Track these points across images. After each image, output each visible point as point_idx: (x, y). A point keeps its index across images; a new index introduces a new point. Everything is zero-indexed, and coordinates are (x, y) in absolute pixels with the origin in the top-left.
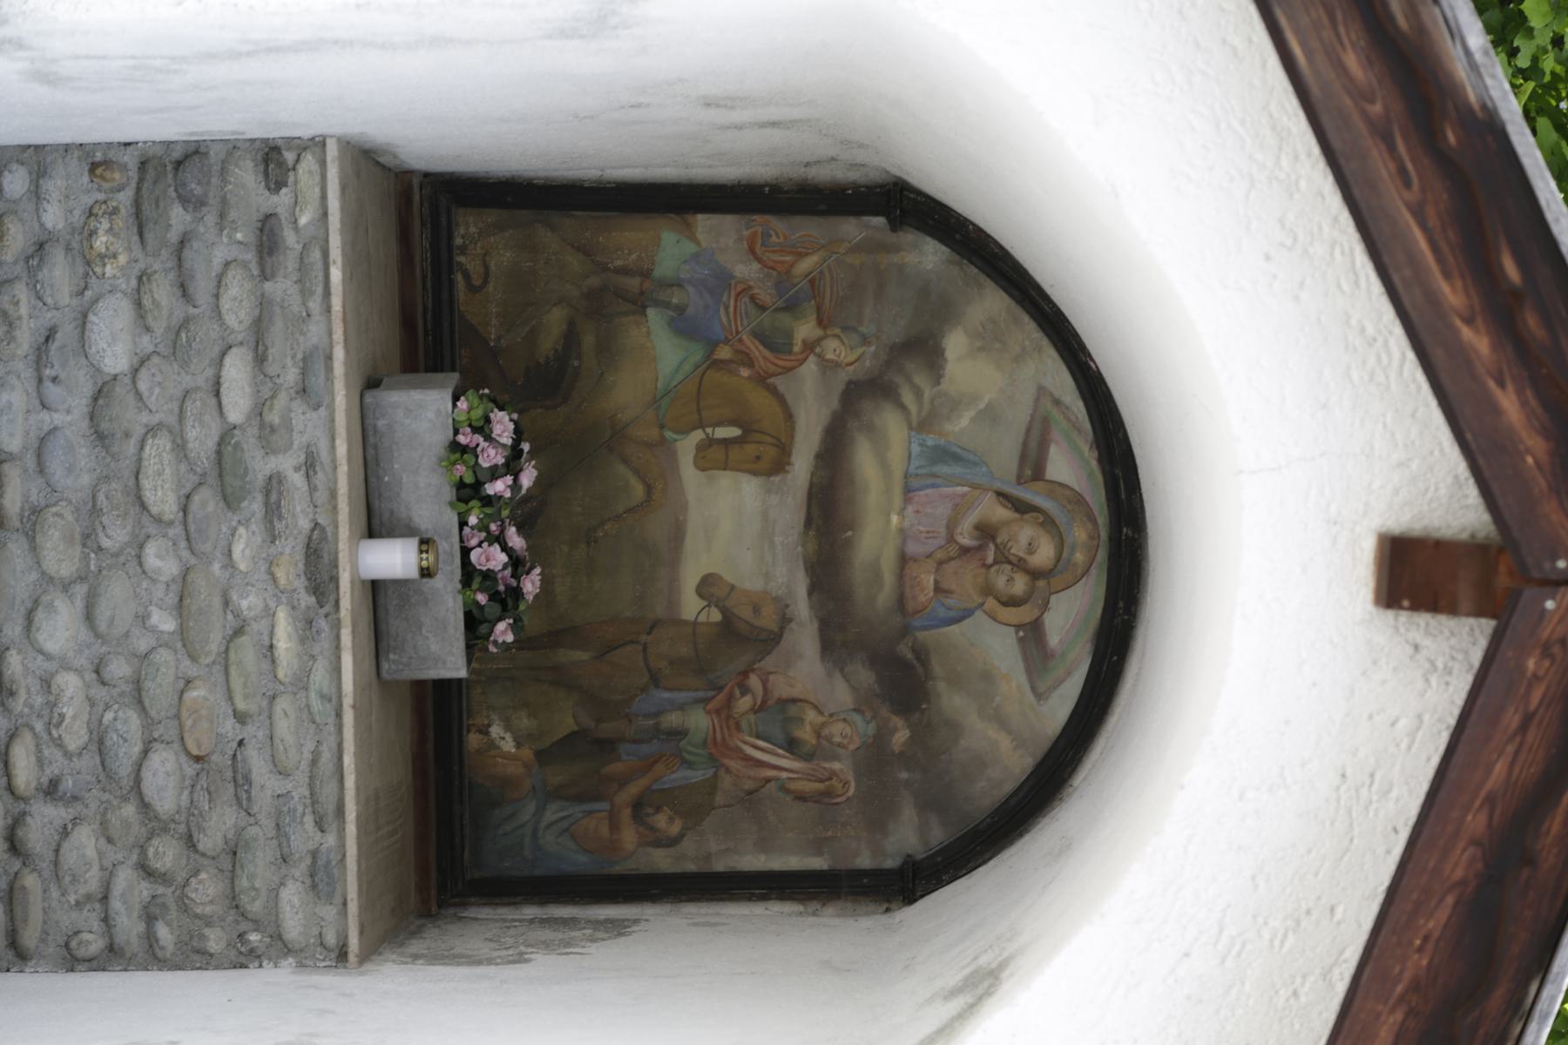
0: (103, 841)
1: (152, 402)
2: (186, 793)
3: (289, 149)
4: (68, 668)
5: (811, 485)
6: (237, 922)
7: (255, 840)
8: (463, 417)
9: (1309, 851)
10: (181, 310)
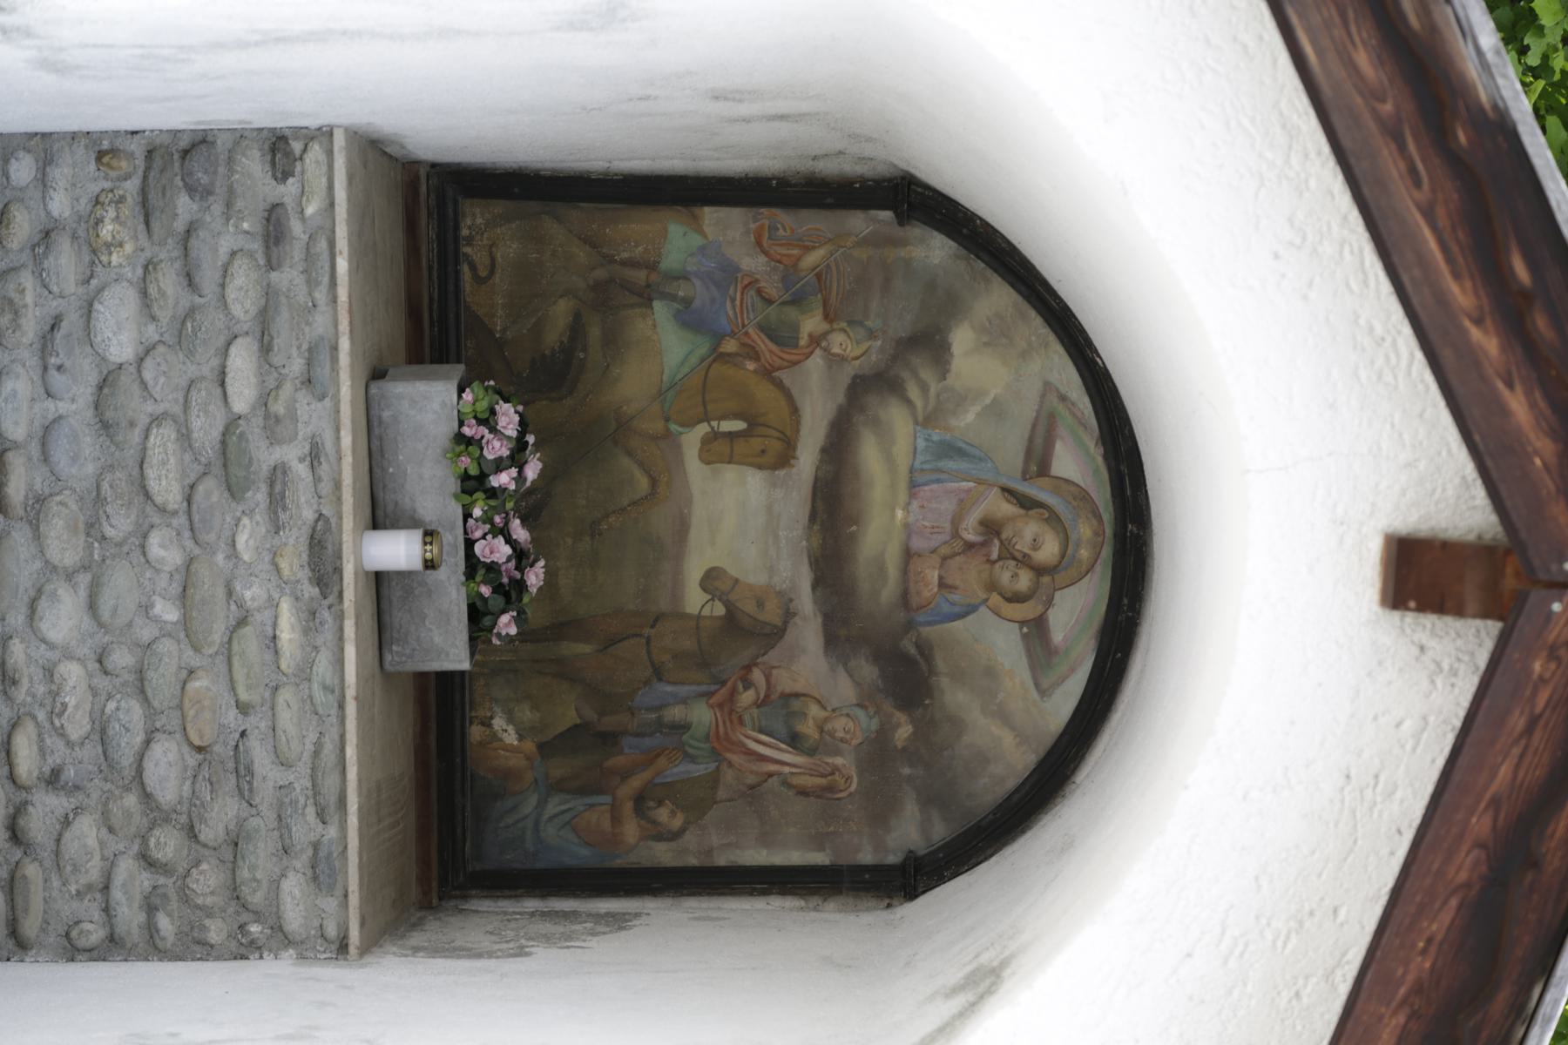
0: (104, 831)
1: (157, 392)
2: (188, 783)
3: (296, 139)
4: (69, 656)
5: (816, 479)
6: (237, 913)
7: (257, 831)
8: (467, 409)
9: (1313, 852)
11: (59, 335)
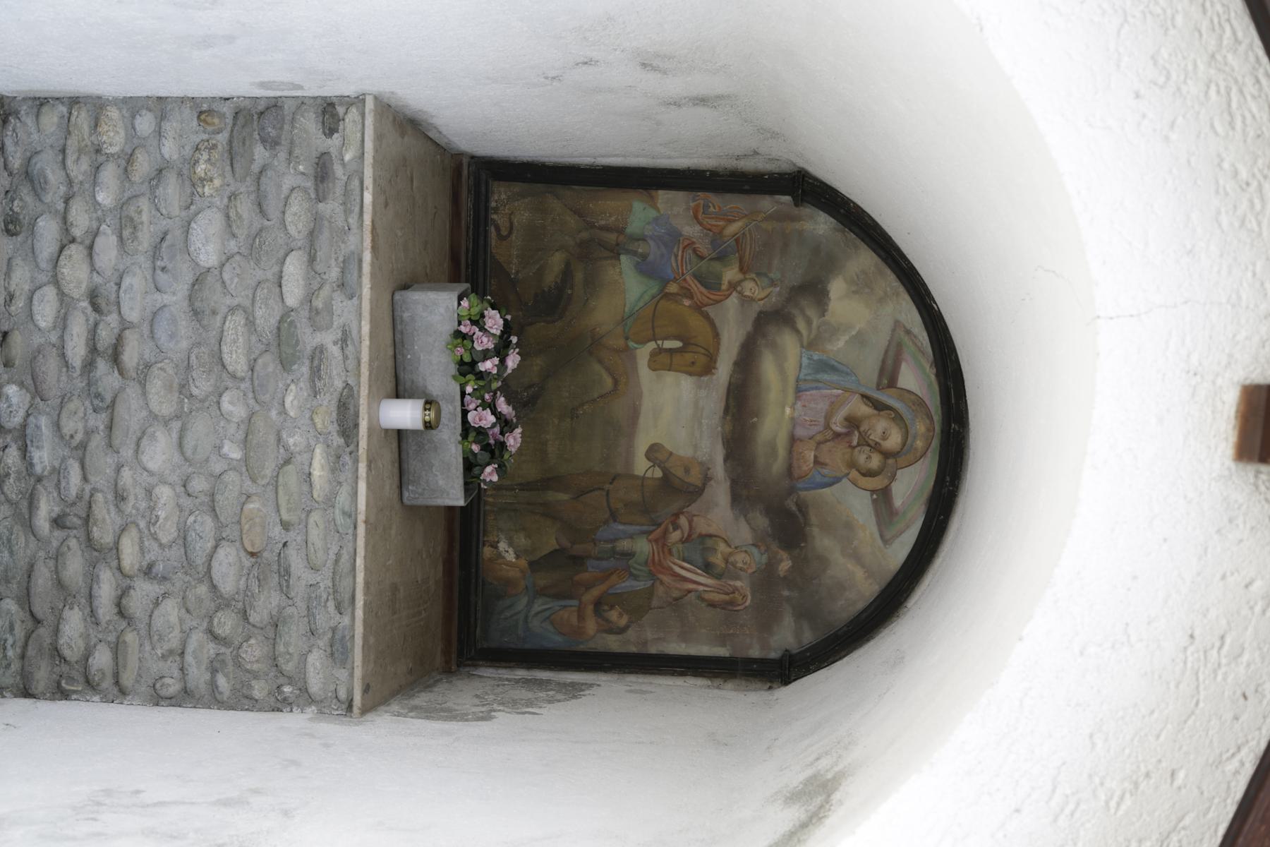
0: (183, 611)
2: (244, 579)
3: (341, 104)
5: (730, 384)
6: (276, 676)
7: (291, 617)
8: (465, 313)
9: (1152, 712)
10: (258, 223)
11: (164, 245)
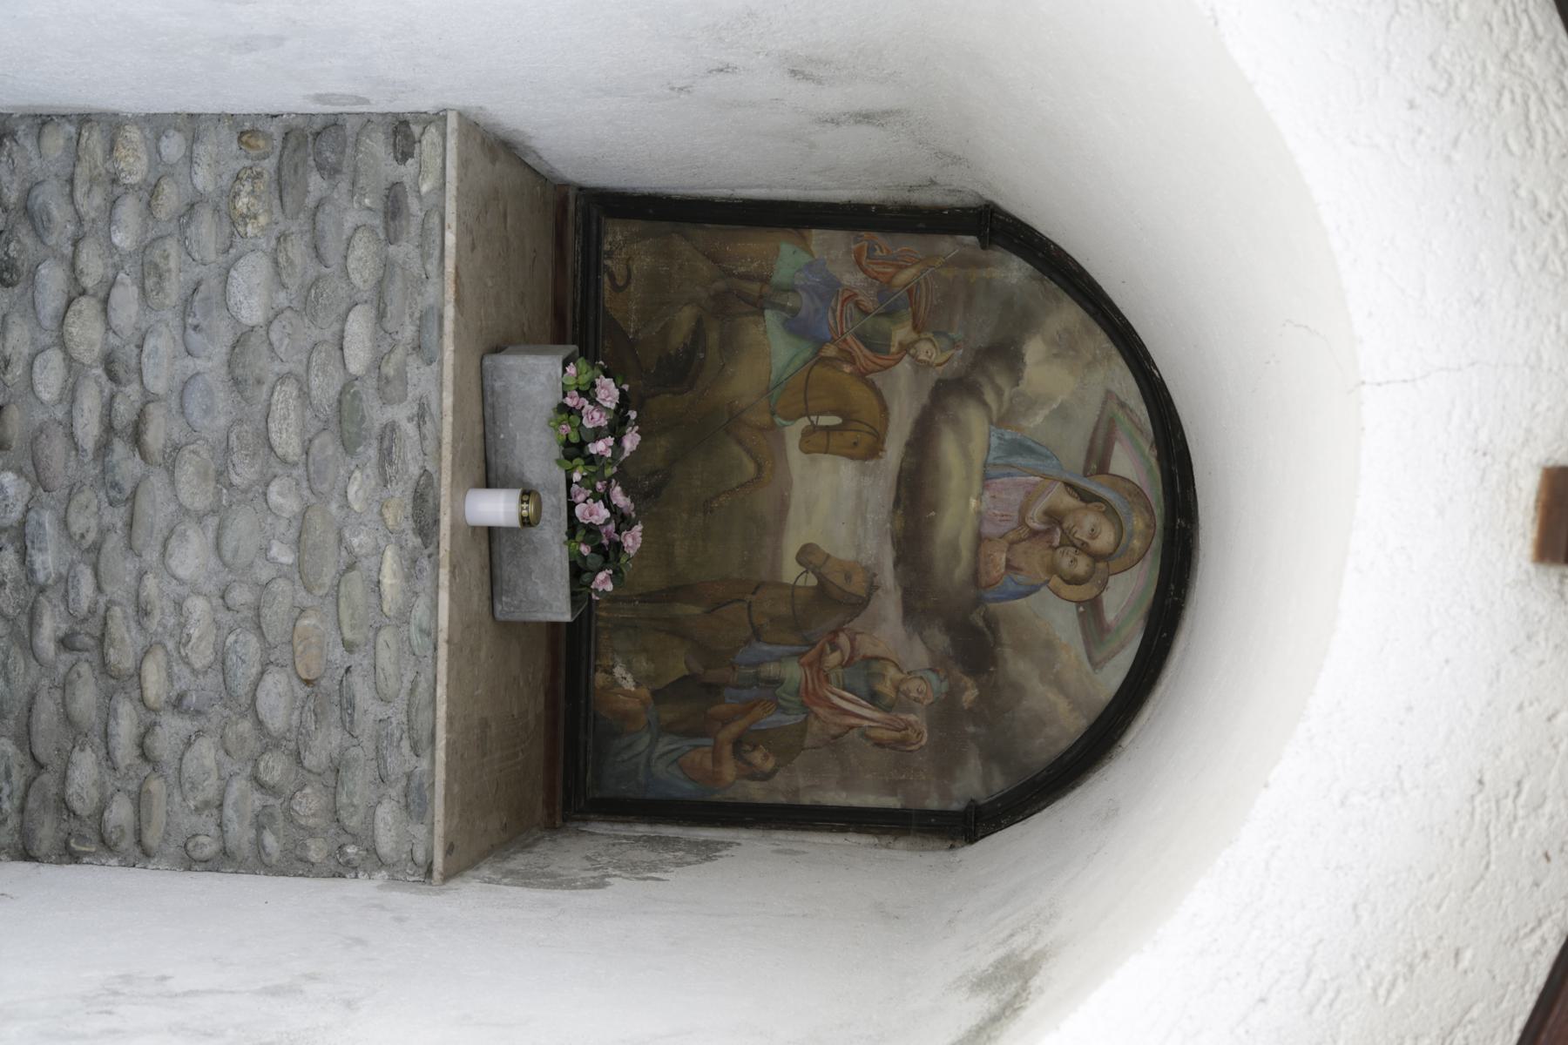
0: (222, 752)
1: (281, 351)
2: (297, 713)
3: (417, 123)
4: (198, 593)
5: (901, 470)
7: (356, 760)
8: (571, 382)
9: (1431, 877)
11: (197, 298)
